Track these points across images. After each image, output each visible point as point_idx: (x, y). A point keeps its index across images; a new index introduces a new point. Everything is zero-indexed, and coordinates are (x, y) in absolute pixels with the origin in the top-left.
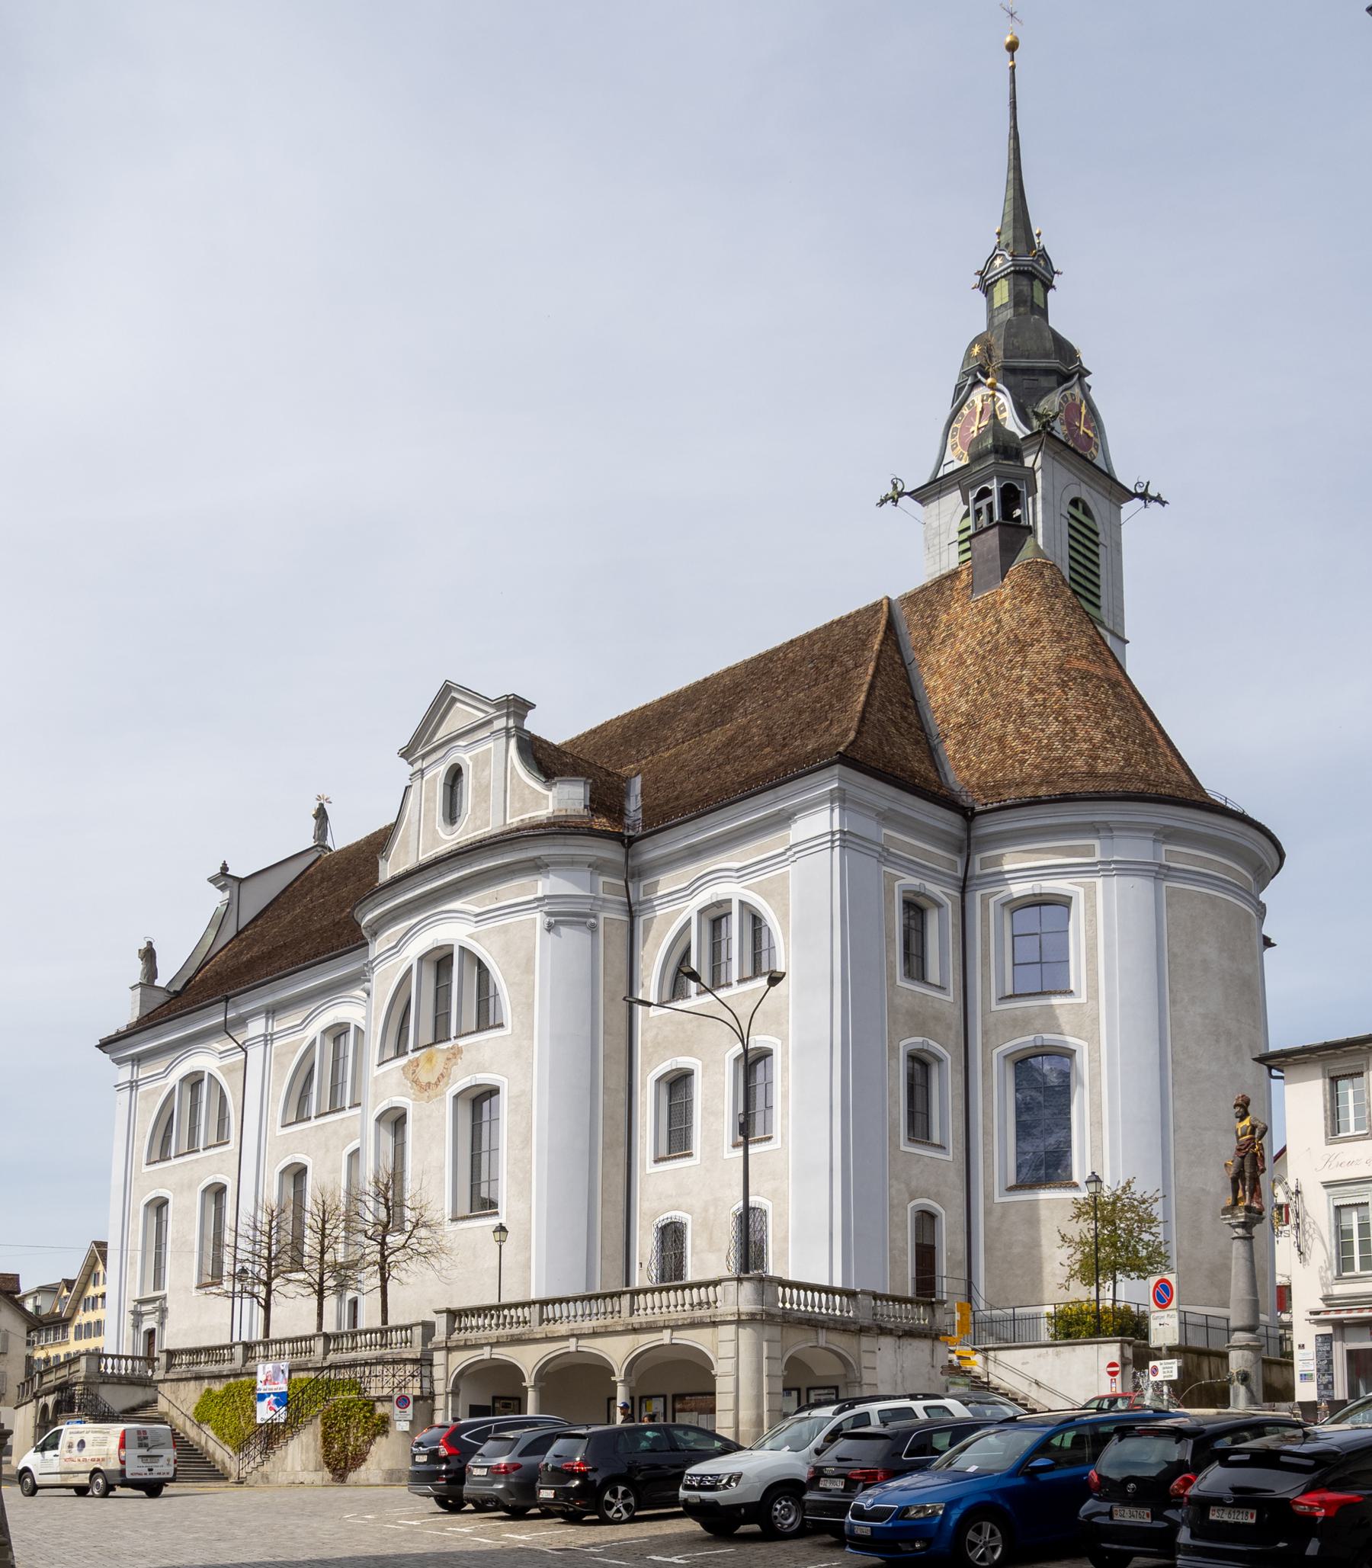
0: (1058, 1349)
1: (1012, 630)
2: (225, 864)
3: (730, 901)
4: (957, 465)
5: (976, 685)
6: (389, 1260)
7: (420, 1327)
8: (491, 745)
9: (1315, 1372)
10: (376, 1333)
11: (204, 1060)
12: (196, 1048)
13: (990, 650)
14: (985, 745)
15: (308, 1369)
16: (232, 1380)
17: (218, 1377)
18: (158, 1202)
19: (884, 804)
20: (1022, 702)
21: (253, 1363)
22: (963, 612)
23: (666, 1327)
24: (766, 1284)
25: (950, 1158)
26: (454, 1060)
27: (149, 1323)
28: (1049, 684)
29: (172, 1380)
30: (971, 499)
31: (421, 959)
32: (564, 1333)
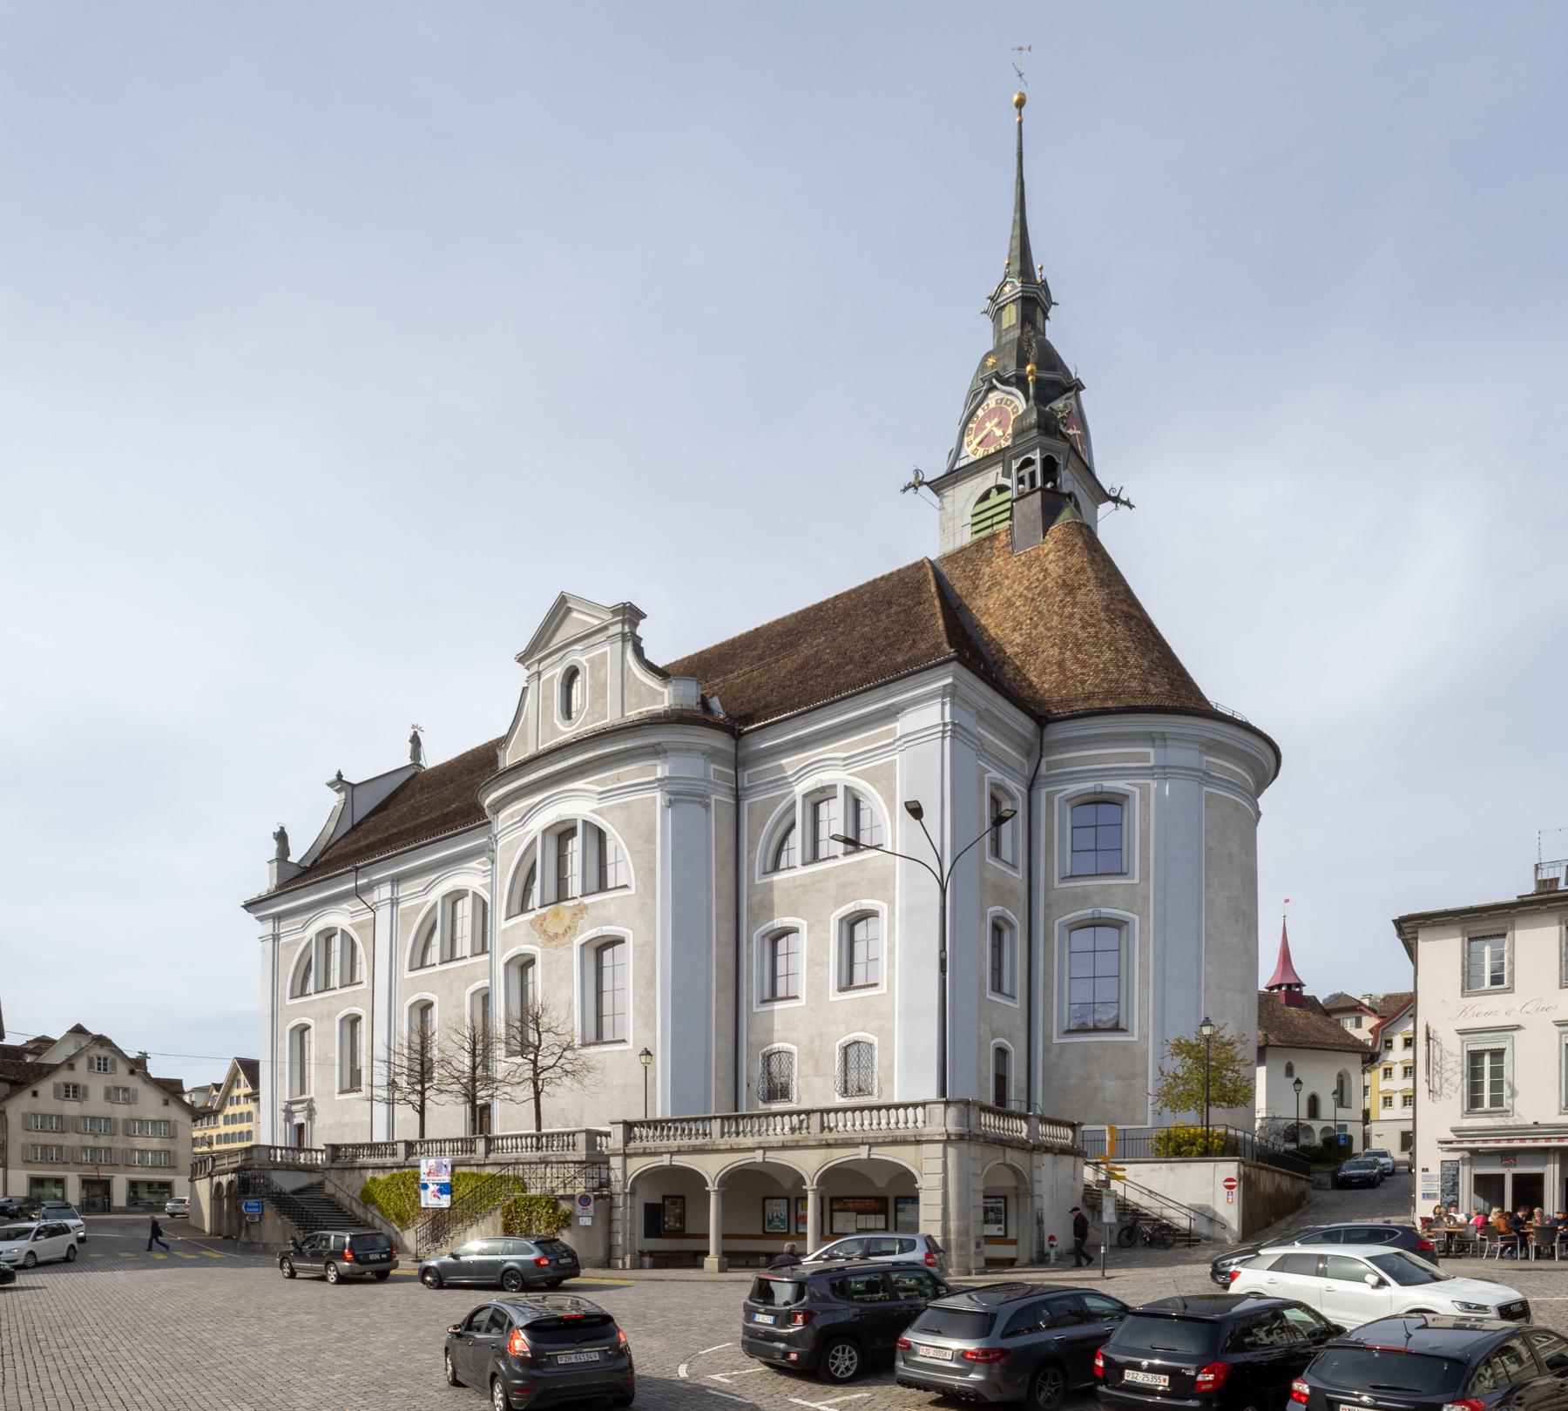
0: (1173, 1165)
1: (1060, 576)
2: (339, 772)
3: (835, 786)
4: (973, 458)
5: (1028, 621)
6: (542, 1076)
7: (584, 1134)
8: (607, 648)
9: (1439, 1192)
10: (532, 1138)
11: (340, 918)
12: (328, 909)
13: (1039, 594)
14: (1046, 669)
15: (471, 1165)
16: (395, 1171)
17: (383, 1168)
18: (423, 1004)
19: (983, 704)
20: (1076, 634)
21: (414, 1158)
22: (1006, 564)
23: (863, 1144)
24: (971, 1107)
25: (1017, 1006)
26: (580, 916)
27: (299, 1119)
28: (1099, 620)
29: (338, 1169)
30: (1014, 467)
31: (544, 832)
32: (751, 1146)
